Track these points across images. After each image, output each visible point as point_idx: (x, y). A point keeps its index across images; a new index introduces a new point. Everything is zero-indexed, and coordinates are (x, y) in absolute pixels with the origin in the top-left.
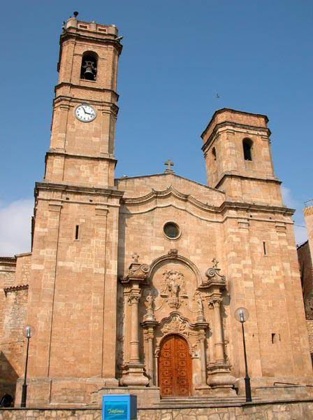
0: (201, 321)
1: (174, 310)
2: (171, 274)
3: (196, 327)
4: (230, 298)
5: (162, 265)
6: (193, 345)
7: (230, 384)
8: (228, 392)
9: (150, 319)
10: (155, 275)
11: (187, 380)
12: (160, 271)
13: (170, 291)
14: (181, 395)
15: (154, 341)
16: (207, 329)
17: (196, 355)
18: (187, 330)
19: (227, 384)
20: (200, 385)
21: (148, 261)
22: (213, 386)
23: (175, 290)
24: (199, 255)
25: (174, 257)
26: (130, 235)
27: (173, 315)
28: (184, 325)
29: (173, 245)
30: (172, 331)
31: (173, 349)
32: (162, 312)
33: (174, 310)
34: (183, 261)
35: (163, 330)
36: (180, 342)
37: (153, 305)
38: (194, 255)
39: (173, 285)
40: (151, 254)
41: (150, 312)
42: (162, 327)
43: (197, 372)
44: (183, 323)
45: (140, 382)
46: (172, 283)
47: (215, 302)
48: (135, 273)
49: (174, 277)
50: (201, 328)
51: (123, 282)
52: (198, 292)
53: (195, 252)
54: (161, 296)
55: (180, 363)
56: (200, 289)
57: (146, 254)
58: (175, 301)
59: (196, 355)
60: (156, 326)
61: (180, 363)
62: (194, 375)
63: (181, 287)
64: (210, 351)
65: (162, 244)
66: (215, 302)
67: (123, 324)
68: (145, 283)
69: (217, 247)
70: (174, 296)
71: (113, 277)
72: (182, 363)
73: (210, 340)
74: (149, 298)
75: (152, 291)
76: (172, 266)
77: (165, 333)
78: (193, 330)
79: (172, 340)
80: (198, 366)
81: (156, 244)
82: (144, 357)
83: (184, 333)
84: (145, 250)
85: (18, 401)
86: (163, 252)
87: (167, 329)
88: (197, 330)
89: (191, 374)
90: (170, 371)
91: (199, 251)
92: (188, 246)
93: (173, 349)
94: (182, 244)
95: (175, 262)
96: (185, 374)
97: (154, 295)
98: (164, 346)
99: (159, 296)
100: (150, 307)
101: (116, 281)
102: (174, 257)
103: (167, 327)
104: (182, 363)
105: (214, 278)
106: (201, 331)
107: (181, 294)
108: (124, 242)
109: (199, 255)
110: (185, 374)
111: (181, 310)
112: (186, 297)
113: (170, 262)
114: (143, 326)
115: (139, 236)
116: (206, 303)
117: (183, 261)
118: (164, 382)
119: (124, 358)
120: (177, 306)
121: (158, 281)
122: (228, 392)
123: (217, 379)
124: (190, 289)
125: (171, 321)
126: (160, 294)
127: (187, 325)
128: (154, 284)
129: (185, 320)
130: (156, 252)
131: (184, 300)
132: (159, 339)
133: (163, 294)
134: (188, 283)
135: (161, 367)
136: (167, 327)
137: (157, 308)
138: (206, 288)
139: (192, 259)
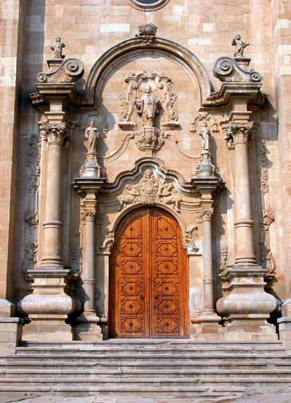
0: (204, 175)
1: (149, 154)
2: (145, 79)
3: (194, 188)
4: (278, 123)
5: (124, 63)
6: (190, 228)
7: (263, 312)
8: (256, 328)
9: (88, 174)
10: (108, 85)
11: (177, 304)
12: (119, 76)
13: (140, 115)
14: (162, 332)
15: (98, 220)
16: (220, 192)
17: (197, 250)
18: (175, 197)
19: (255, 312)
20: (200, 313)
21: (89, 59)
22: (225, 317)
23: (149, 111)
24: (208, 35)
25: (148, 43)
26: (57, 6)
27: (143, 165)
28: (170, 185)
29: (150, 18)
30: (142, 200)
31: (146, 236)
32: (121, 159)
33: (149, 154)
34: (168, 51)
35: (122, 198)
36: (163, 222)
37: (99, 145)
38: (197, 36)
39: (146, 102)
40: (102, 42)
41: (91, 160)
42: (120, 191)
43: (196, 285)
44: (167, 181)
45: (52, 307)
46: (145, 97)
47: (236, 130)
48: (49, 79)
49: (152, 84)
50: (206, 191)
51: (28, 102)
52: (203, 114)
53: (200, 28)
54: (121, 127)
55: (162, 267)
56: (207, 108)
57: (90, 42)
58: (148, 136)
59: (197, 250)
60: (104, 190)
61: (162, 267)
62: (192, 290)
63: (164, 106)
64: (227, 241)
65: (126, 19)
66: (236, 130)
67: (36, 187)
68: (80, 101)
69: (252, 16)
70: (149, 126)
71: (6, 92)
72: (167, 267)
73: (229, 218)
74: (91, 132)
75: (99, 119)
76: (146, 64)
77: (127, 203)
78: (191, 195)
79: (146, 218)
80: (200, 268)
81: (114, 20)
82: (81, 255)
83: (169, 203)
84: (86, 36)
85: (19, 348)
86: (126, 34)
87: (130, 195)
88: (198, 195)
89: (187, 291)
90: (140, 285)
91: (208, 27)
92: (184, 19)
93: (146, 236)
94: (171, 14)
95: (153, 55)
96: (172, 289)
97: (105, 126)
98: (128, 232)
99: (116, 127)
100: (91, 150)
101: (13, 99)
102: (148, 43)
103: (132, 192)
104: (167, 267)
105: (233, 78)
106: (204, 196)
107: (164, 120)
108: (43, 21)
109: (208, 35)
110: (172, 289)
111: (164, 155)
112: (177, 127)
113: (143, 54)
114: (71, 189)
115: (74, 7)
116: (221, 138)
117: (168, 51)
118: (127, 308)
119: (37, 258)
120: (155, 145)
121: (115, 96)
122: (256, 328)
123: (231, 300)
124: (187, 107)
125: (141, 176)
126: (118, 122)
127: (177, 184)
128: (105, 103)
129: (170, 175)
130: (112, 36)
131: (172, 133)
132: (113, 218)
133: (125, 122)
134: (181, 96)
135: (119, 275)
136: (132, 192)
137: (110, 153)
138: (220, 104)
139: (192, 44)
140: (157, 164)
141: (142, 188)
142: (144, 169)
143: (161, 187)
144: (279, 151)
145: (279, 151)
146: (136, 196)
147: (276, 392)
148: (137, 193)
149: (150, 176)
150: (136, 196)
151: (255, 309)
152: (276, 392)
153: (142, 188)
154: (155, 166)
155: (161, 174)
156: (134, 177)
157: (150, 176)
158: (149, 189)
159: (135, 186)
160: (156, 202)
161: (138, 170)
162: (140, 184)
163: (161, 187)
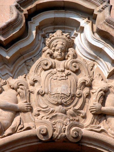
140: (90, 15)
141: (37, 88)
142: (45, 30)
143: (99, 85)
144: (112, 11)
145: (112, 11)
146: (16, 112)
147: (78, 40)
148: (21, 104)
149: (65, 51)
150: (16, 112)
151: (62, 5)
152: (78, 40)
153: (37, 88)
154: (83, 22)
155: (100, 45)
156: (14, 50)
157: (65, 51)
158: (61, 88)
159: (13, 82)
160: (85, 132)
161: (25, 33)
162: (32, 75)
163: (99, 85)
